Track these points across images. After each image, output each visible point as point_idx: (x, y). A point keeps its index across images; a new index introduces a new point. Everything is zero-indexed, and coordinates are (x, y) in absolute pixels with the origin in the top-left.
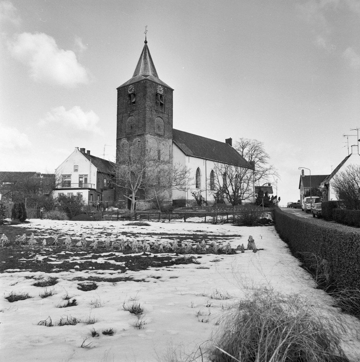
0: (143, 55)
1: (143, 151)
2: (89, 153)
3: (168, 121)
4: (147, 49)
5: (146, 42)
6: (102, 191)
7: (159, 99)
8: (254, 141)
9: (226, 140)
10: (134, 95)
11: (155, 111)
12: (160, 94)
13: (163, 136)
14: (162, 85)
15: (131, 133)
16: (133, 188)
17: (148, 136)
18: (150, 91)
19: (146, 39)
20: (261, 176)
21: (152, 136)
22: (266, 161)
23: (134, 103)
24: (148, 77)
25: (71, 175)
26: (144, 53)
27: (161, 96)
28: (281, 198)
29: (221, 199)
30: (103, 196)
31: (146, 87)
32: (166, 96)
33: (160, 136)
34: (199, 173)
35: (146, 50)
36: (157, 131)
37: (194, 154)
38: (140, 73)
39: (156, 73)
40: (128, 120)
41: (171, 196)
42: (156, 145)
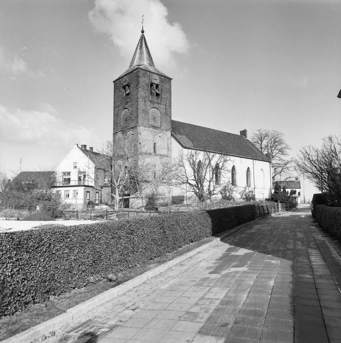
0: (139, 44)
1: (135, 144)
2: (92, 150)
3: (166, 112)
4: (143, 39)
5: (143, 32)
6: (102, 188)
7: (155, 88)
8: (273, 132)
9: (241, 132)
10: (128, 85)
11: (150, 101)
12: (155, 84)
13: (160, 128)
14: (157, 74)
15: (126, 127)
16: (116, 184)
17: (141, 129)
18: (144, 81)
19: (143, 28)
20: (282, 170)
21: (146, 129)
22: (287, 154)
23: (128, 94)
24: (141, 66)
25: (70, 172)
26: (140, 42)
27: (157, 86)
28: (301, 193)
29: (229, 195)
30: (102, 193)
31: (138, 77)
32: (162, 86)
33: (155, 127)
34: (235, 171)
35: (142, 39)
36: (151, 122)
37: (194, 146)
38: (135, 63)
39: (153, 63)
40: (123, 113)
41: (169, 192)
42: (151, 138)
